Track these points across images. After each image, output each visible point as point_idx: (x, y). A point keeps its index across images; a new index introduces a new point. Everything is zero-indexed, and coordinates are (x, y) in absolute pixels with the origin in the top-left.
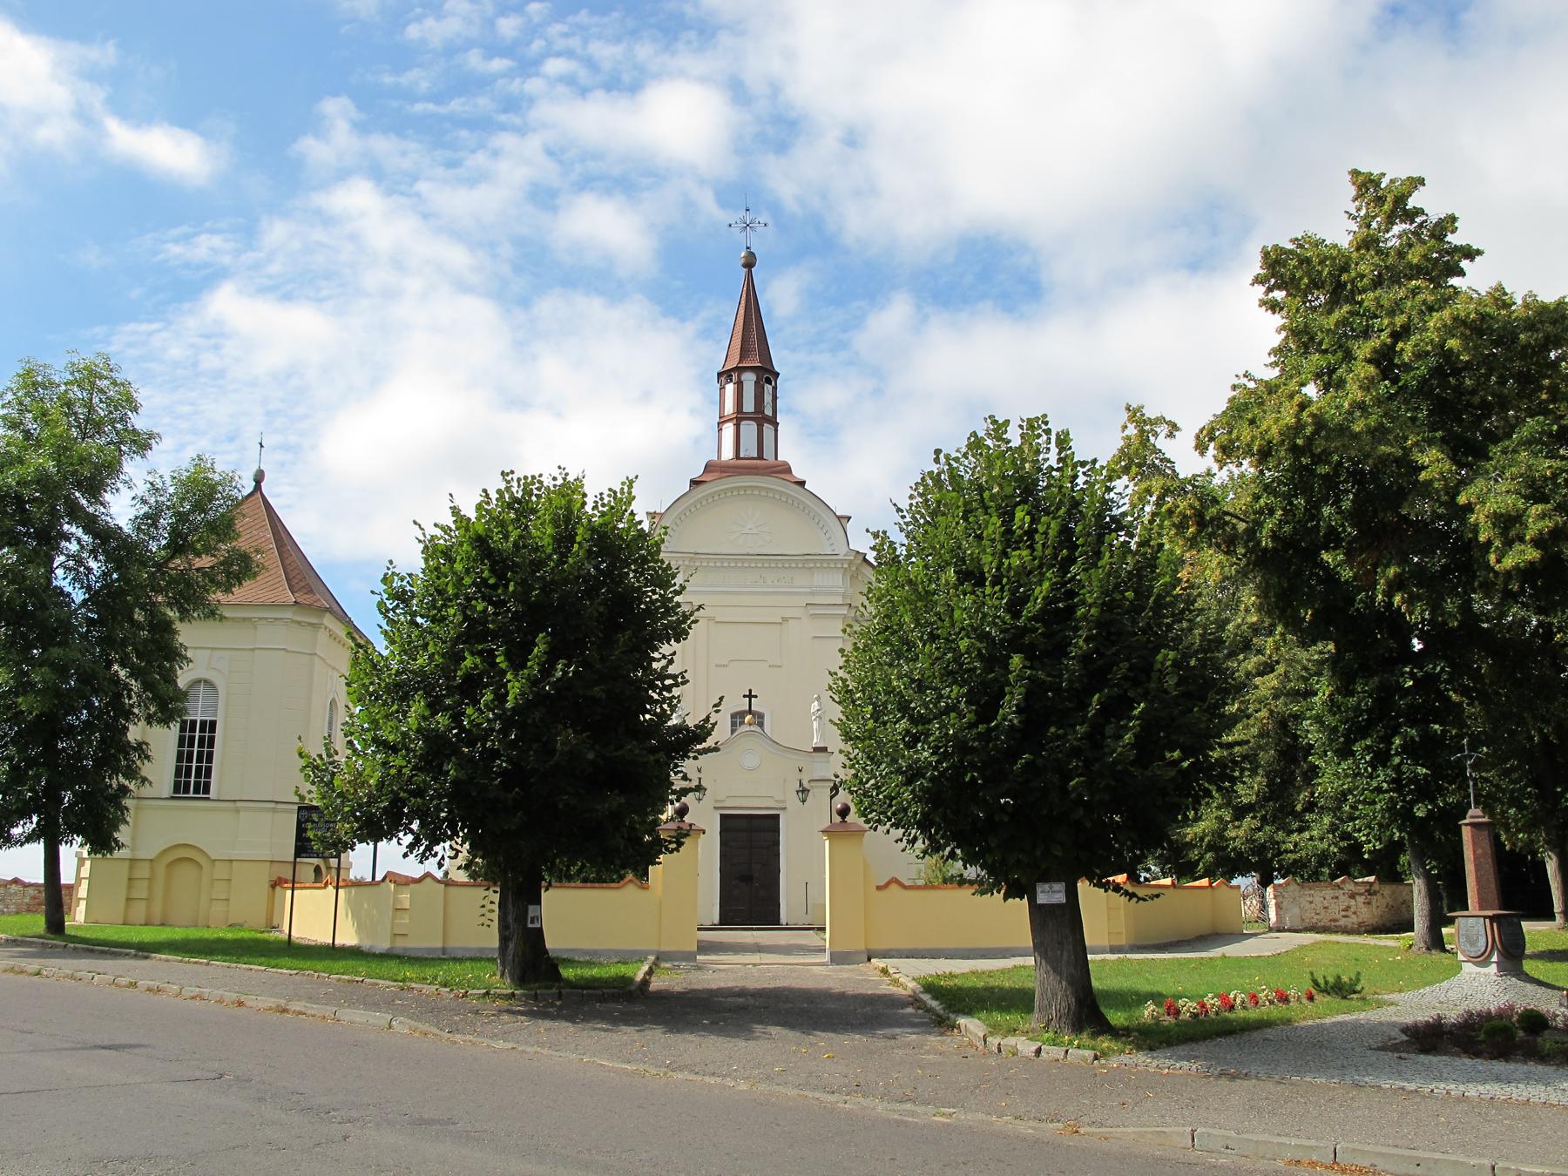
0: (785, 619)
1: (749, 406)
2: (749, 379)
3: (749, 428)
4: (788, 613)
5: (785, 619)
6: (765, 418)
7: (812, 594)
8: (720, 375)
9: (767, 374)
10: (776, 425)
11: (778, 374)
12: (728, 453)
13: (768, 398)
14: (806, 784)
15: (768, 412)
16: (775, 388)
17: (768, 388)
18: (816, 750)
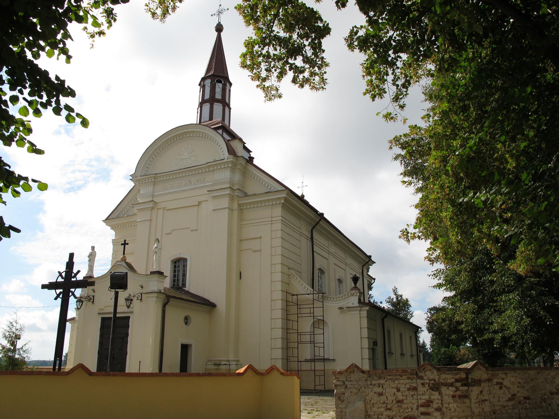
0: (200, 203)
3: (218, 107)
4: (201, 199)
5: (200, 203)
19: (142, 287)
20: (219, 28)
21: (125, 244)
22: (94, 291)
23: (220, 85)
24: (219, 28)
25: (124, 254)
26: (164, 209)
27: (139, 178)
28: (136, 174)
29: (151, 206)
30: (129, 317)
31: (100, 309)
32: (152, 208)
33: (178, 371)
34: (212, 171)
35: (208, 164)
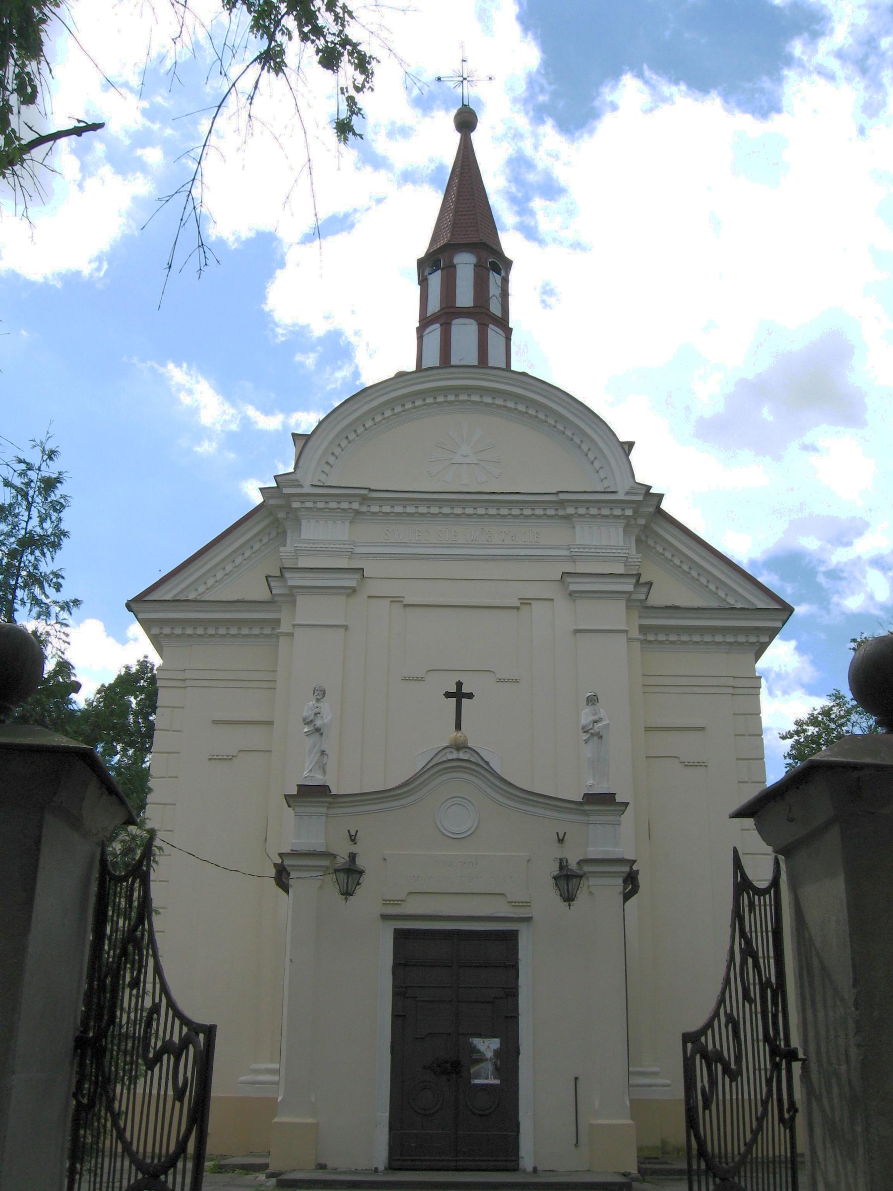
0: (526, 602)
1: (465, 297)
3: (465, 333)
4: (530, 591)
5: (526, 602)
6: (492, 317)
7: (572, 559)
8: (421, 263)
9: (495, 263)
10: (508, 332)
12: (433, 359)
13: (494, 290)
14: (573, 865)
15: (495, 308)
16: (505, 281)
17: (494, 279)
18: (592, 799)
19: (561, 841)
21: (459, 695)
22: (353, 839)
25: (458, 726)
26: (396, 600)
27: (307, 490)
29: (353, 584)
30: (517, 931)
31: (387, 902)
32: (352, 591)
33: (476, 363)
34: (568, 517)
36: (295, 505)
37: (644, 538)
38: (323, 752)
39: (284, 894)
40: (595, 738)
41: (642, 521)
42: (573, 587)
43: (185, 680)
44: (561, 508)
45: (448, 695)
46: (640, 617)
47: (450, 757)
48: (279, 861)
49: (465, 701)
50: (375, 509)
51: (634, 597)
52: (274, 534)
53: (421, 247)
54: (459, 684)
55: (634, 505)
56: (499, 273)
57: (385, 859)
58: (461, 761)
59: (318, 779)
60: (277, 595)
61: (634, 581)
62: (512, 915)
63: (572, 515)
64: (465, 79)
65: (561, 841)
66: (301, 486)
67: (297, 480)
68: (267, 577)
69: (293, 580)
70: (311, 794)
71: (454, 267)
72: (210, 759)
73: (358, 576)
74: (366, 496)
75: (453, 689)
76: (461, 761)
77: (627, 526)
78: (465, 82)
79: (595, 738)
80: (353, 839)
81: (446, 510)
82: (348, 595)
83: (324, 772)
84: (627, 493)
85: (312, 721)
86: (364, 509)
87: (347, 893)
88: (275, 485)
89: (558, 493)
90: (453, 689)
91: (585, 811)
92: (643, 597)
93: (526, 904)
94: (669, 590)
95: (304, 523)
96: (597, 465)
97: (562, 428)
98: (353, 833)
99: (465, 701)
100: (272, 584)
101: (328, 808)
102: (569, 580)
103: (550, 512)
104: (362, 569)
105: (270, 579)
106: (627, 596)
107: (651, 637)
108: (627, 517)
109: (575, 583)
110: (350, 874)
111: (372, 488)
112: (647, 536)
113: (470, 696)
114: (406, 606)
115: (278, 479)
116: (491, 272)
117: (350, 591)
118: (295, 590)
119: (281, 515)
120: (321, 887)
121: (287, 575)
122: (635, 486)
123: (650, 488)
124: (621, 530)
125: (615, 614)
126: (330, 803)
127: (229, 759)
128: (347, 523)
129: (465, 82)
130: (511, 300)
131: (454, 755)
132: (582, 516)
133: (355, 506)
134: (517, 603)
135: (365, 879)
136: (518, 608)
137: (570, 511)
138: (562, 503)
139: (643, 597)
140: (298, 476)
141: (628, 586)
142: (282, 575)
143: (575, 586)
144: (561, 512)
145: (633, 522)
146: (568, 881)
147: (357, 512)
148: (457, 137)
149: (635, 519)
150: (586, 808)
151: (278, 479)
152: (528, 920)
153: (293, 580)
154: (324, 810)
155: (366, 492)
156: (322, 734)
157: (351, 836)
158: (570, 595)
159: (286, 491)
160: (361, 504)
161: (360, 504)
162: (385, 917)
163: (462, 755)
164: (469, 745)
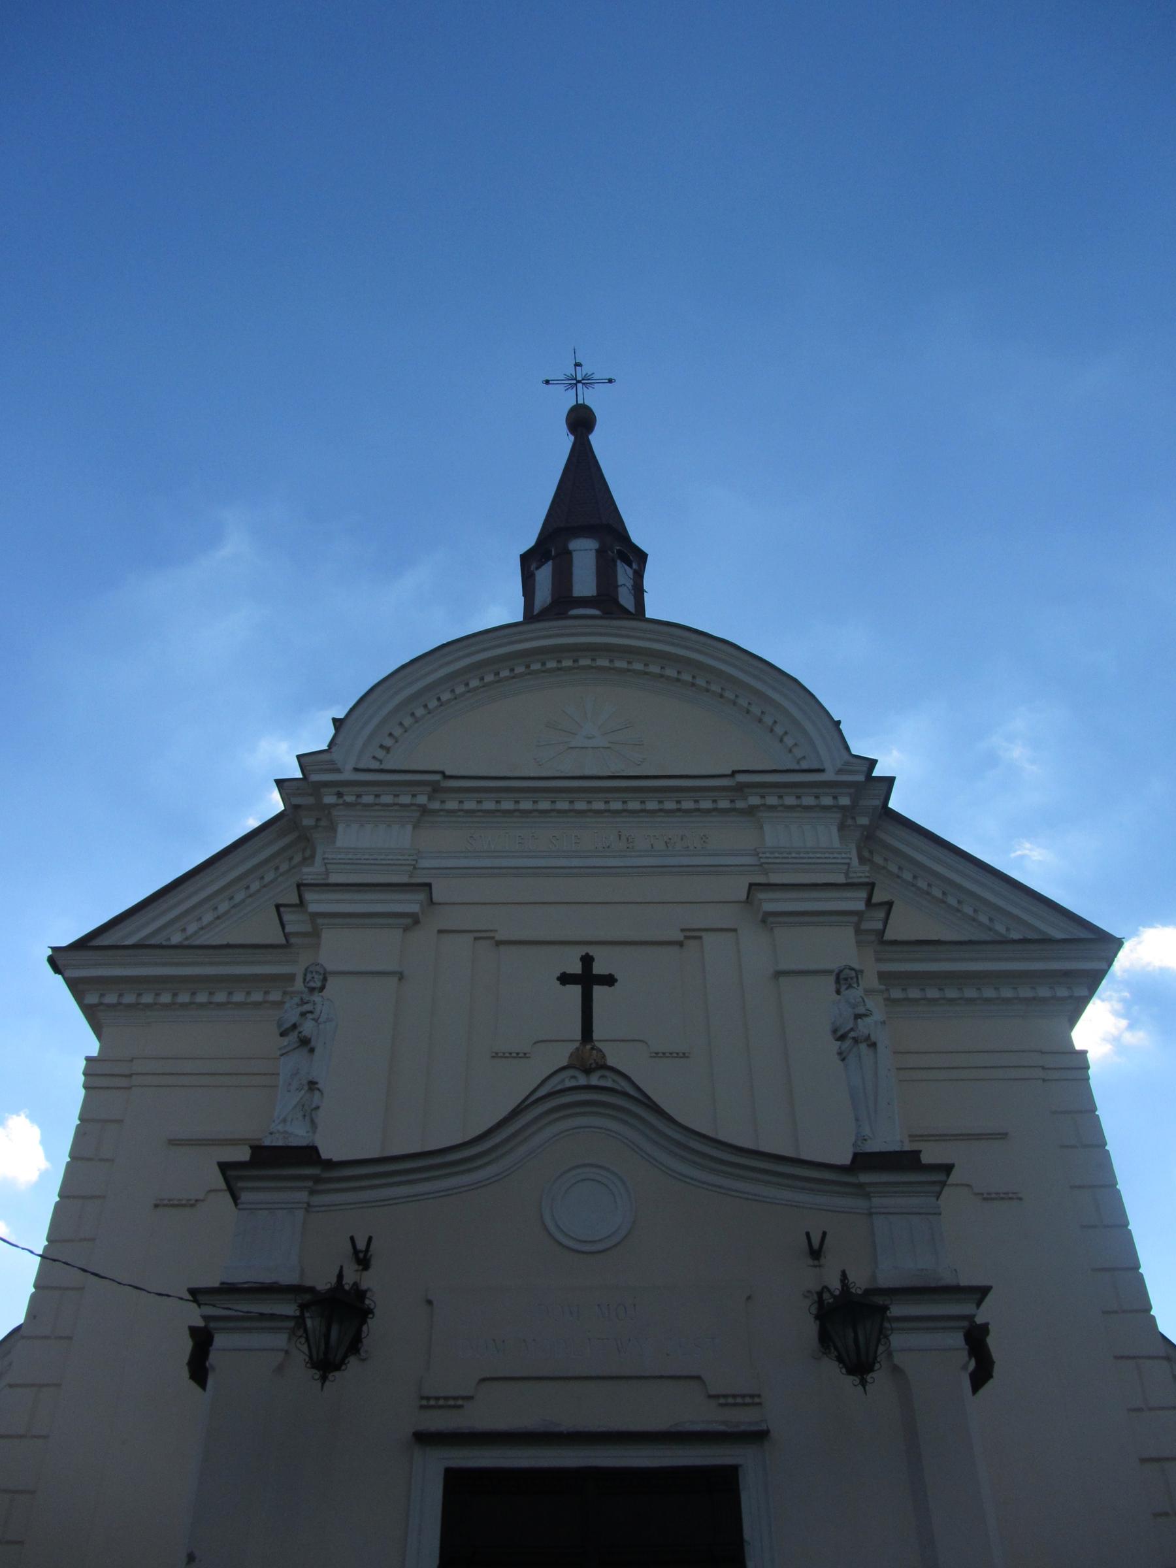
0: (693, 935)
1: (584, 582)
2: (584, 554)
5: (693, 935)
8: (526, 559)
11: (642, 557)
15: (626, 599)
16: (639, 575)
17: (624, 574)
18: (864, 1161)
19: (816, 1254)
20: (581, 421)
23: (630, 572)
24: (581, 421)
26: (481, 936)
27: (348, 775)
28: (336, 755)
29: (414, 908)
31: (428, 1403)
34: (751, 811)
35: (741, 778)
36: (329, 799)
37: (866, 854)
38: (312, 1085)
39: (199, 1390)
40: (863, 1047)
41: (864, 821)
42: (768, 907)
43: (130, 1076)
44: (739, 795)
45: (565, 979)
46: (878, 960)
47: (569, 1083)
48: (201, 1324)
49: (598, 991)
50: (452, 805)
51: (865, 926)
52: (297, 859)
53: (529, 540)
54: (587, 961)
55: (852, 791)
56: (630, 566)
57: (430, 1302)
58: (590, 1083)
59: (298, 1135)
60: (297, 934)
61: (864, 894)
62: (722, 1428)
63: (757, 807)
64: (579, 382)
65: (816, 1254)
66: (338, 771)
67: (332, 762)
68: (278, 907)
69: (317, 903)
70: (274, 1163)
71: (569, 553)
72: (156, 1206)
73: (421, 896)
74: (439, 784)
75: (576, 968)
76: (590, 1083)
77: (842, 827)
78: (580, 385)
79: (863, 1047)
80: (363, 1260)
81: (563, 805)
82: (406, 929)
83: (314, 1125)
84: (840, 771)
85: (294, 1026)
86: (436, 805)
87: (326, 1364)
88: (300, 776)
89: (734, 773)
90: (576, 968)
91: (860, 1186)
92: (880, 926)
93: (752, 1400)
94: (907, 924)
95: (341, 828)
96: (789, 741)
97: (732, 697)
98: (361, 1245)
99: (598, 991)
100: (286, 918)
101: (312, 1192)
102: (761, 896)
103: (724, 804)
104: (429, 885)
105: (282, 909)
106: (855, 919)
107: (896, 994)
108: (843, 808)
109: (771, 900)
110: (334, 1321)
111: (447, 773)
112: (871, 852)
113: (609, 980)
114: (499, 943)
115: (303, 760)
116: (619, 563)
117: (409, 921)
118: (320, 921)
119: (308, 822)
120: (280, 1369)
121: (309, 896)
122: (854, 760)
123: (873, 763)
124: (834, 830)
125: (838, 947)
126: (317, 1180)
127: (193, 1204)
128: (409, 827)
129: (580, 385)
130: (647, 598)
131: (582, 1080)
132: (772, 808)
133: (422, 799)
134: (680, 936)
135: (374, 1328)
136: (680, 944)
137: (754, 800)
138: (741, 788)
139: (880, 926)
140: (336, 755)
141: (855, 902)
142: (302, 903)
143: (771, 903)
144: (740, 804)
145: (850, 822)
146: (851, 1326)
147: (424, 811)
148: (565, 442)
149: (854, 818)
150: (864, 1178)
151: (303, 760)
152: (759, 1437)
153: (317, 903)
154: (303, 1196)
155: (438, 777)
156: (312, 1050)
157: (356, 1252)
158: (764, 921)
159: (314, 778)
160: (433, 795)
161: (429, 799)
162: (424, 1438)
163: (594, 1080)
164: (610, 1062)
